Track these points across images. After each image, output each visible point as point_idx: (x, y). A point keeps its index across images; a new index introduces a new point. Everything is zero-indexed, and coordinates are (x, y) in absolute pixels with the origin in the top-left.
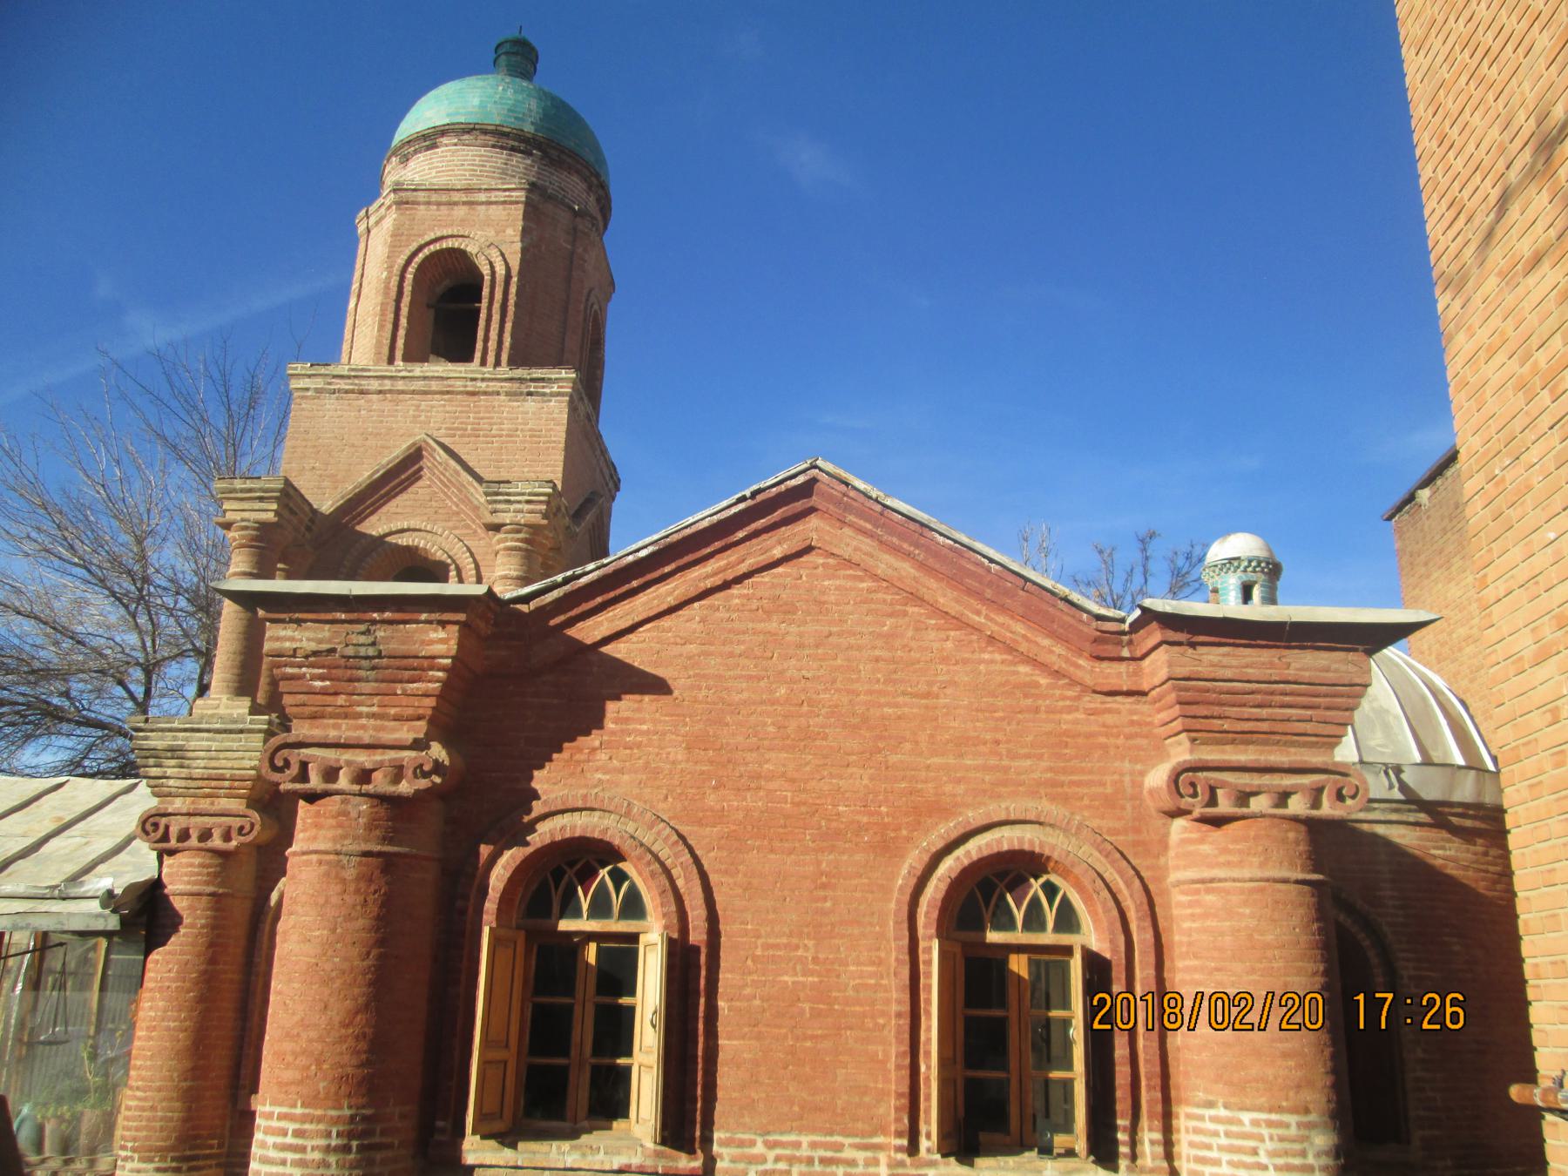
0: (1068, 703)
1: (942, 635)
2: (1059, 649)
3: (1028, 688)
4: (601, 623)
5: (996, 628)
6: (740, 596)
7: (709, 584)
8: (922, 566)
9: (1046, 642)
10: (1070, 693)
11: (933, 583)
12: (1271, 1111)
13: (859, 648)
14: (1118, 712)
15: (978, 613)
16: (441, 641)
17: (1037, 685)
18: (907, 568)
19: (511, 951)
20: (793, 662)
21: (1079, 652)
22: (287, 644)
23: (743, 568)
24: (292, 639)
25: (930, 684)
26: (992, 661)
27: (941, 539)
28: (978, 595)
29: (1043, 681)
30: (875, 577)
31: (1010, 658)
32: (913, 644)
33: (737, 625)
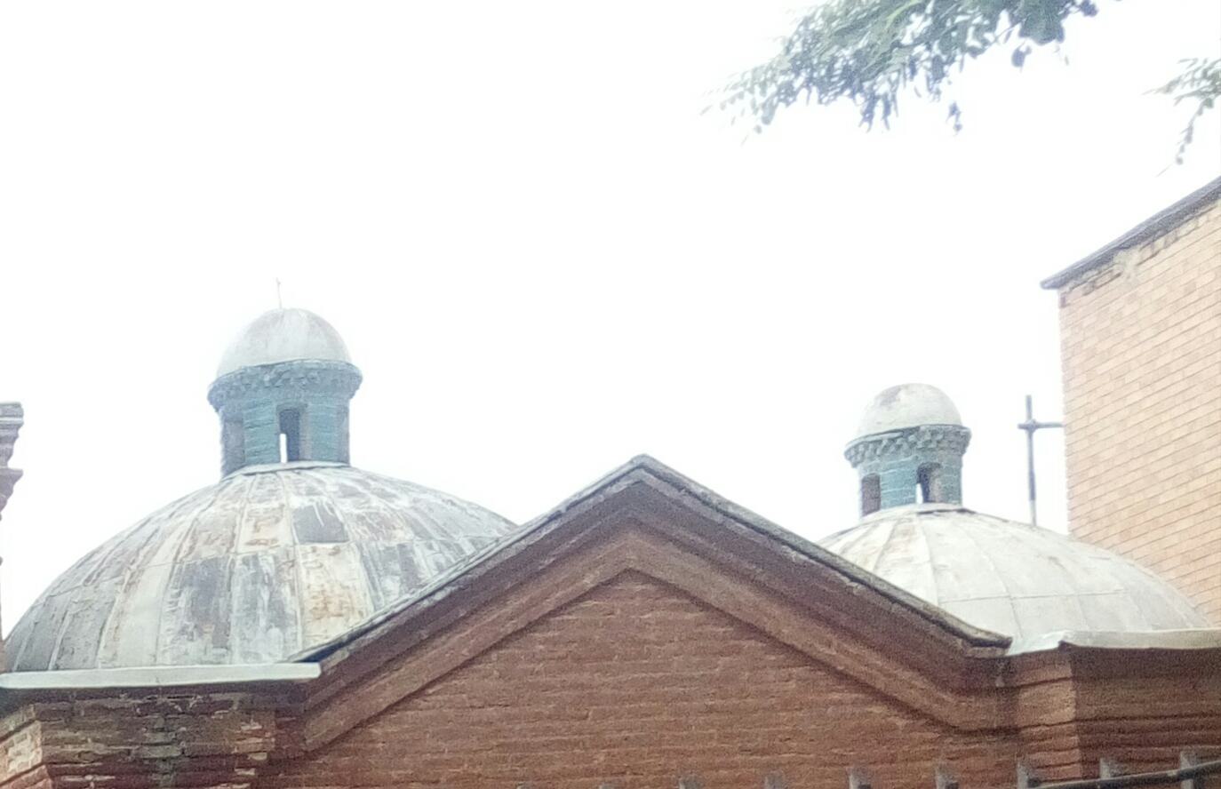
0: (927, 747)
1: (784, 673)
2: (920, 683)
3: (882, 733)
4: (384, 688)
5: (849, 661)
6: (545, 642)
7: (510, 628)
8: (761, 587)
9: (907, 675)
10: (930, 735)
11: (775, 610)
12: (1085, 778)
13: (687, 698)
14: (983, 754)
15: (829, 645)
16: (255, 734)
17: (894, 728)
18: (745, 594)
19: (1079, 775)
20: (612, 720)
21: (944, 685)
22: (70, 748)
23: (549, 605)
24: (73, 742)
25: (772, 736)
26: (841, 703)
27: (794, 554)
28: (828, 621)
29: (901, 723)
30: (705, 606)
31: (861, 696)
32: (752, 688)
33: (543, 679)
